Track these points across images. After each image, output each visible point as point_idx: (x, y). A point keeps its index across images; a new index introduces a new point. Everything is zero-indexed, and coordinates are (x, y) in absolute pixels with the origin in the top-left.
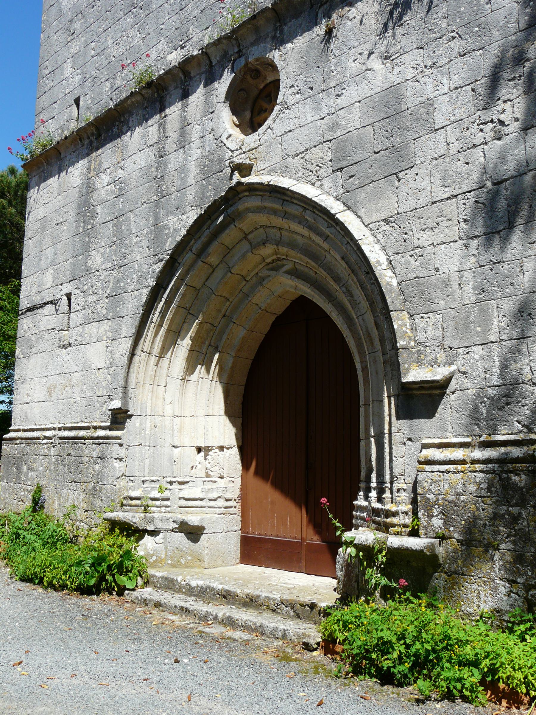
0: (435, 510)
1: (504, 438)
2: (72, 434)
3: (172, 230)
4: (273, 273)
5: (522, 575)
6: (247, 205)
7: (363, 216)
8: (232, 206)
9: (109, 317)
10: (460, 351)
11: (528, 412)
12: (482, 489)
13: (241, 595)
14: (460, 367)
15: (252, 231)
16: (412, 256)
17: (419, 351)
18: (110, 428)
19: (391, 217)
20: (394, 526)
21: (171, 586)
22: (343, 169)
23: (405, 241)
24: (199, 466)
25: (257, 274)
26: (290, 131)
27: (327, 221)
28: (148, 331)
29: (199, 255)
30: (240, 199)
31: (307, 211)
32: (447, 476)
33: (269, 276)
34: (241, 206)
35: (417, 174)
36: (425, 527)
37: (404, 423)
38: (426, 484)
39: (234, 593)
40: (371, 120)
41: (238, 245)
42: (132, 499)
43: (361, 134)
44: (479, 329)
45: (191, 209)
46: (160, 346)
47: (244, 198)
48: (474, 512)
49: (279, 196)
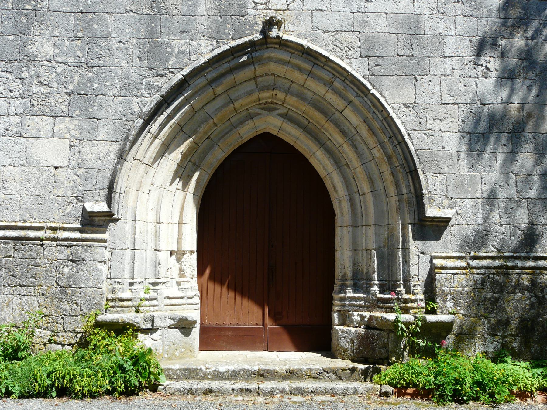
0: (448, 297)
1: (485, 254)
2: (22, 233)
3: (176, 50)
4: (264, 112)
5: (501, 331)
6: (273, 55)
7: (387, 97)
8: (256, 51)
9: (74, 115)
10: (458, 201)
11: (498, 240)
12: (478, 284)
13: (280, 371)
14: (458, 210)
15: (262, 76)
16: (425, 134)
17: (430, 197)
18: (81, 231)
19: (410, 104)
20: (413, 308)
21: (193, 375)
22: (370, 57)
23: (420, 123)
24: (173, 268)
25: (247, 109)
26: (321, 10)
27: (356, 92)
28: (143, 140)
29: (210, 83)
30: (267, 48)
31: (337, 79)
32: (456, 277)
33: (260, 114)
34: (267, 54)
35: (430, 81)
36: (441, 308)
37: (419, 243)
38: (442, 281)
39: (274, 371)
40: (396, 31)
41: (245, 84)
42: (122, 300)
43: (387, 37)
44: (470, 189)
45: (202, 38)
46: (154, 156)
47: (272, 49)
48: (473, 298)
49: (312, 59)
